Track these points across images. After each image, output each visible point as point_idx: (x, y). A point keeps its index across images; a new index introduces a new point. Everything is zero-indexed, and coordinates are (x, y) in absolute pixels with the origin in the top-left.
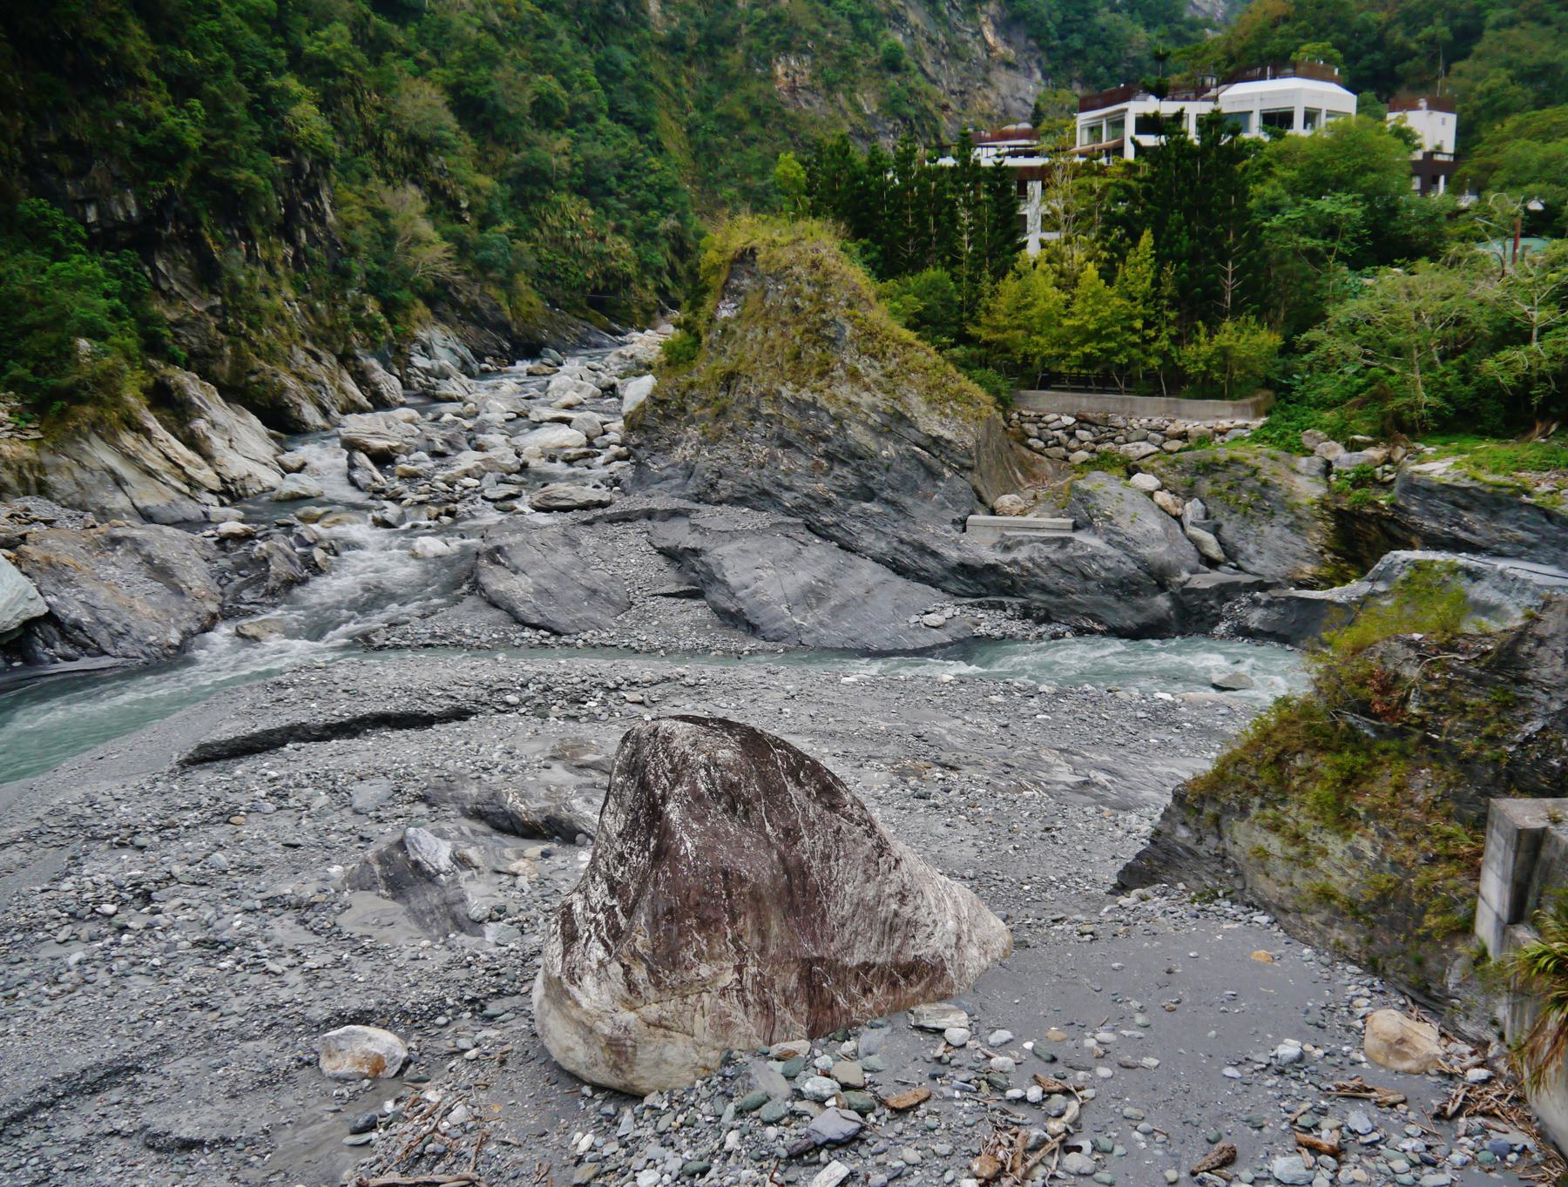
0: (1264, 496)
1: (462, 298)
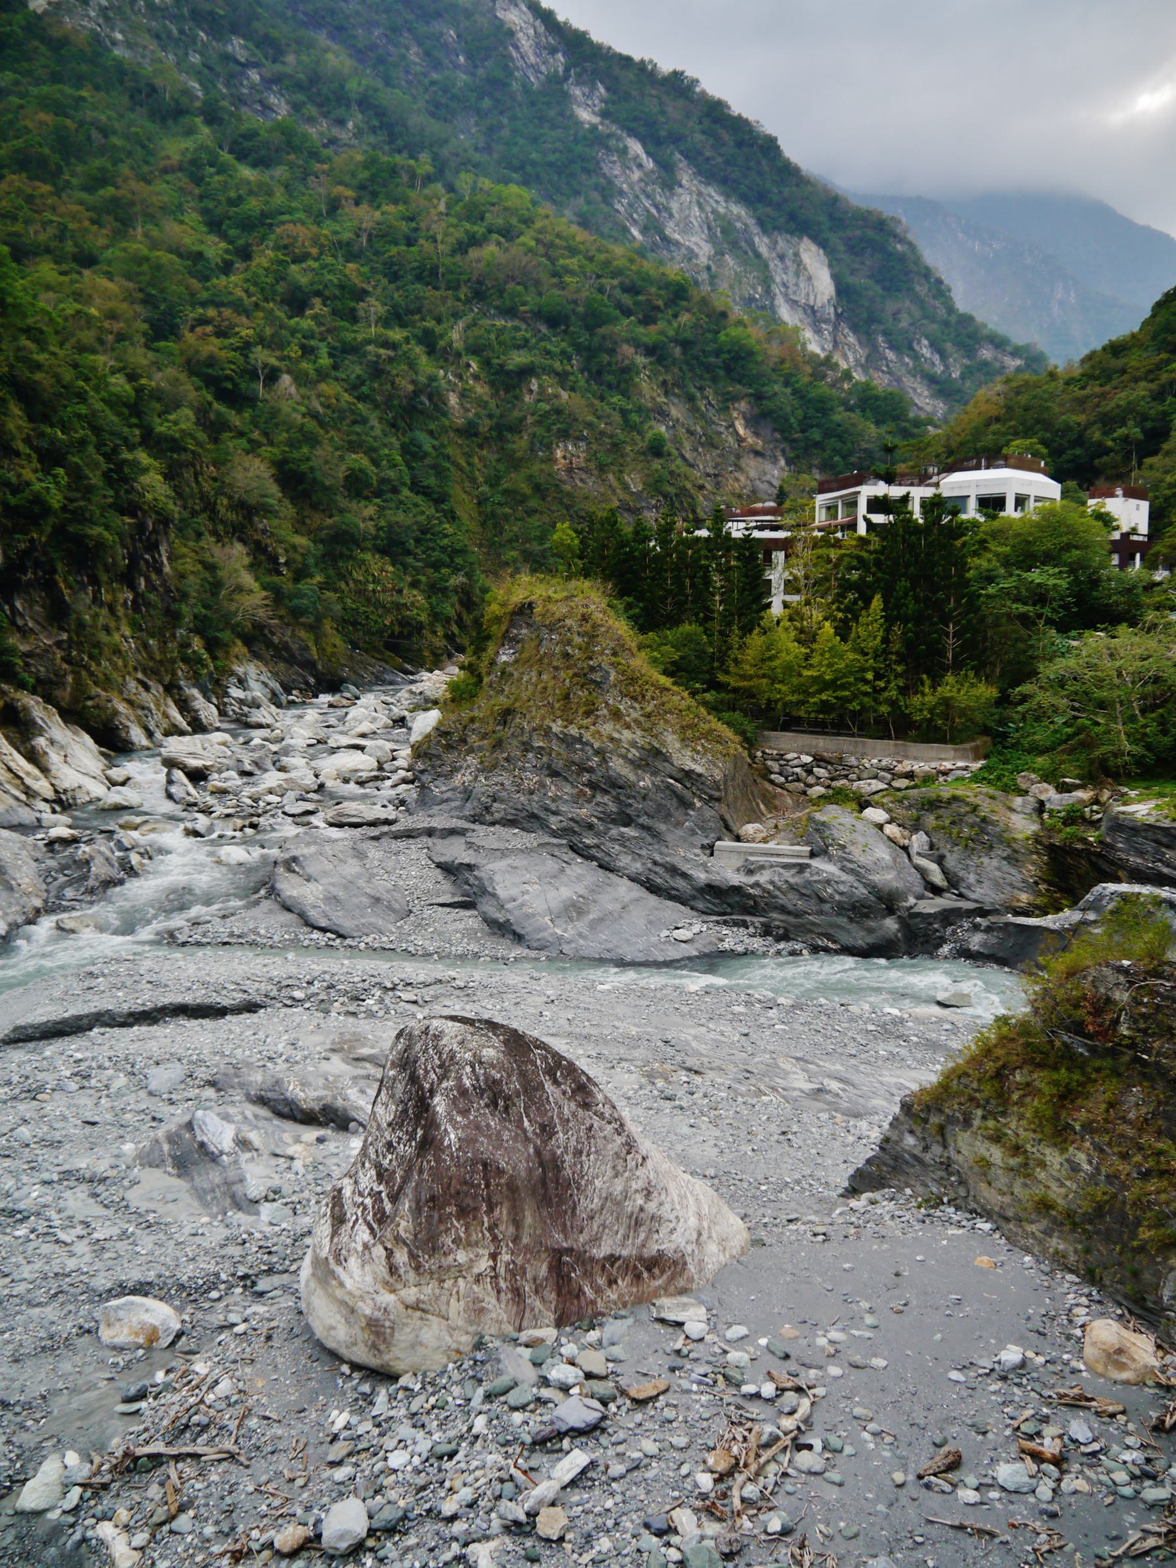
1: (276, 640)
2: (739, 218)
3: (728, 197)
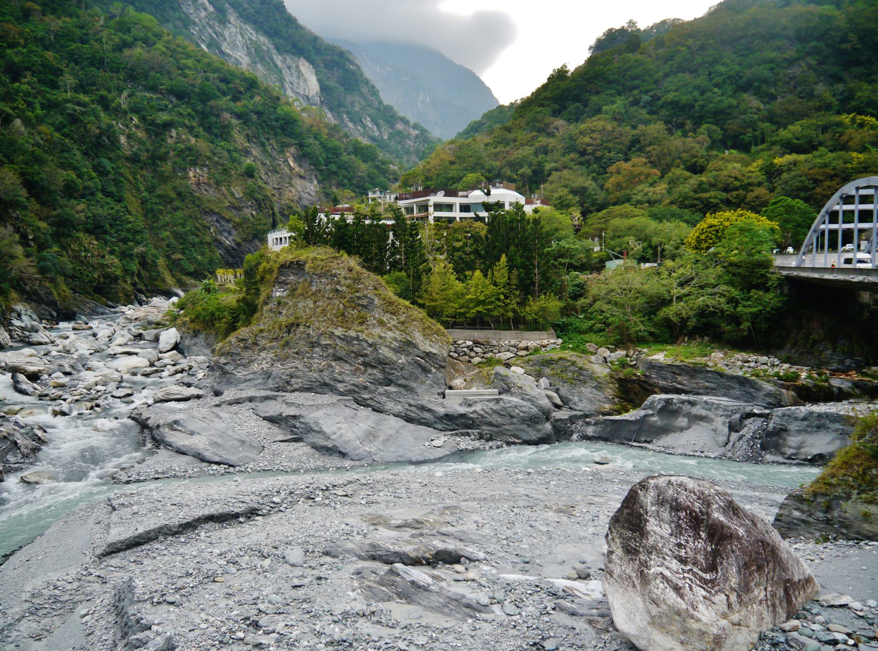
0: (581, 374)
1: (28, 288)
2: (264, 44)
3: (257, 32)
